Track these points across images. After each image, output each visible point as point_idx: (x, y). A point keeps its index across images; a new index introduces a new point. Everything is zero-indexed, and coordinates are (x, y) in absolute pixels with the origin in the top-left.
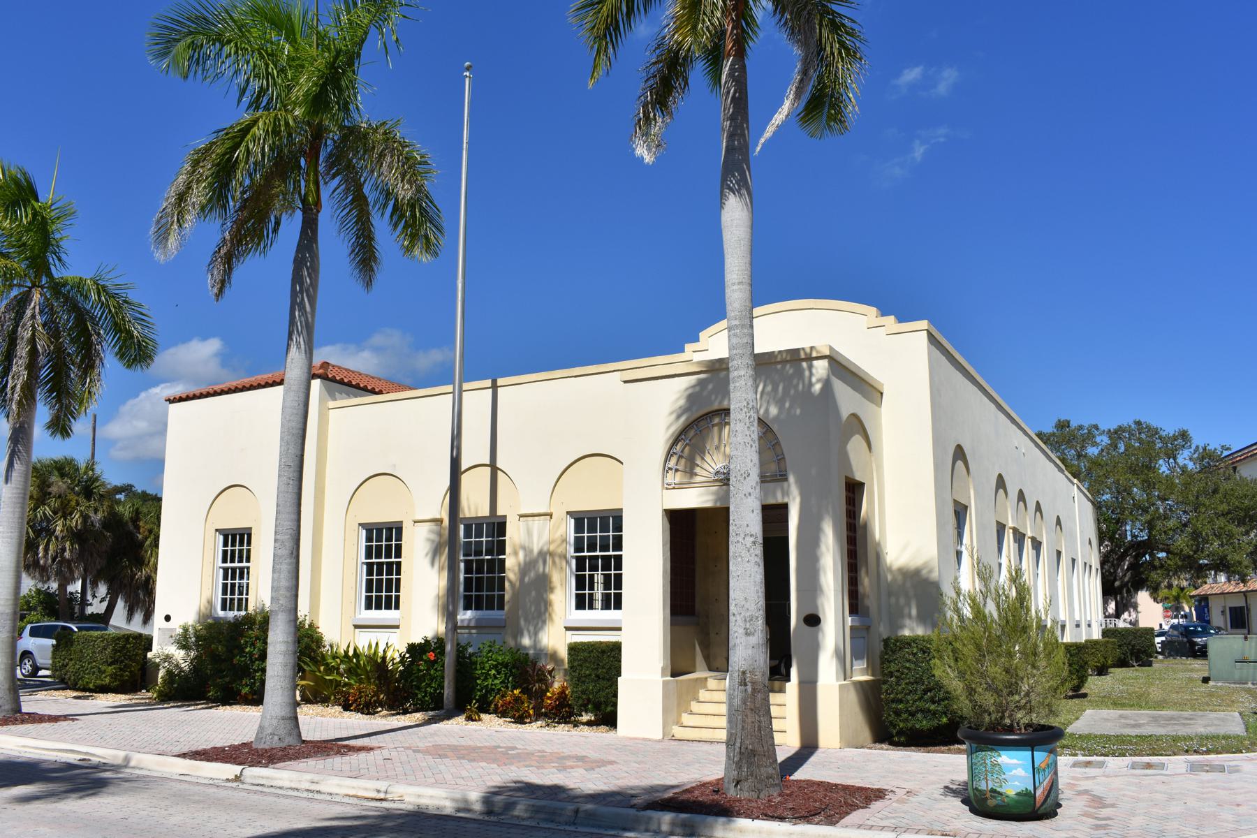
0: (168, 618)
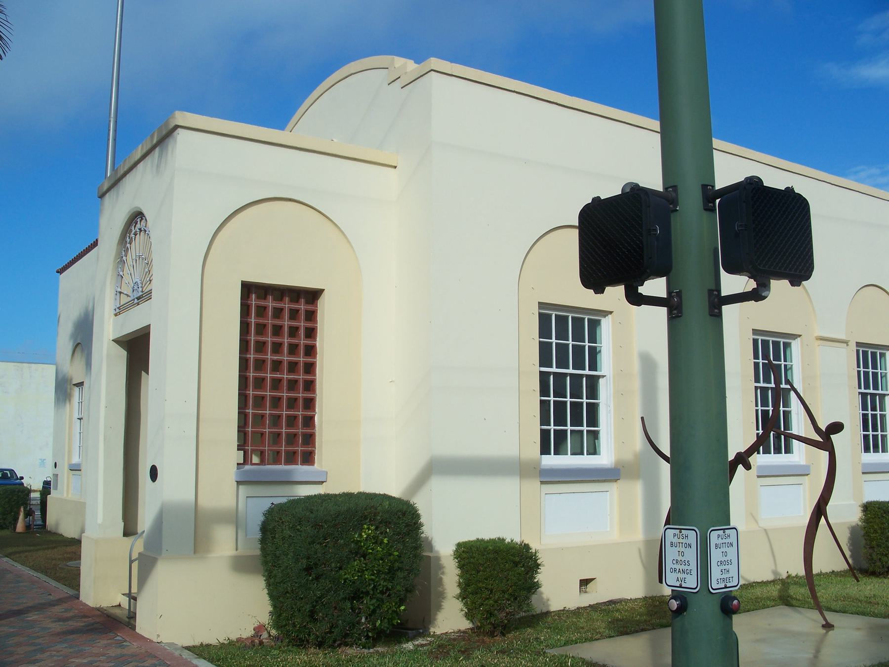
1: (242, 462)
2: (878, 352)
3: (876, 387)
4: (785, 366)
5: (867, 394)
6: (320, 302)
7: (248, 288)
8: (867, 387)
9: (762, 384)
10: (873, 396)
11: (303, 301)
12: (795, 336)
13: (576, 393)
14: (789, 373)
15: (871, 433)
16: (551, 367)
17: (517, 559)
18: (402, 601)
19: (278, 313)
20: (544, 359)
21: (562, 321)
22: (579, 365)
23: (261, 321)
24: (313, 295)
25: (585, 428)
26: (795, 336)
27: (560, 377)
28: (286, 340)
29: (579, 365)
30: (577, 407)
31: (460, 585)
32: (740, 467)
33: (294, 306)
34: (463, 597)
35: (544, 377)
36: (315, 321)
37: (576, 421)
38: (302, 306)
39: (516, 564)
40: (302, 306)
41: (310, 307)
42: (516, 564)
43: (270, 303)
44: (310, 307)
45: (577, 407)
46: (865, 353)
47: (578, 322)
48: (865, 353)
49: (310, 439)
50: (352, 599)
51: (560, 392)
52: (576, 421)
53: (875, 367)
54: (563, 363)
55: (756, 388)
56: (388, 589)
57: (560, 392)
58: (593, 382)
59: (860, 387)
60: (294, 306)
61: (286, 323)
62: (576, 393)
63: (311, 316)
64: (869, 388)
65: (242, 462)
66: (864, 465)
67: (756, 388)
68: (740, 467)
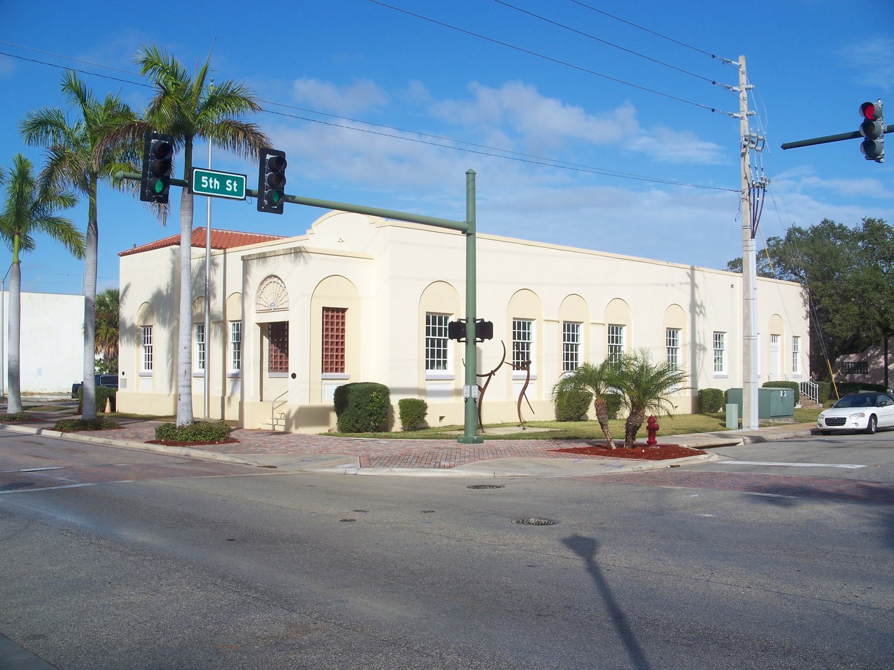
0: (123, 373)
1: (527, 371)
2: (517, 321)
3: (573, 341)
4: (577, 335)
5: (617, 346)
6: (346, 313)
7: (324, 309)
8: (670, 345)
9: (566, 342)
10: (672, 348)
11: (340, 313)
12: (533, 320)
13: (439, 346)
14: (621, 339)
15: (570, 361)
16: (436, 336)
17: (420, 405)
18: (384, 418)
19: (332, 316)
20: (428, 334)
21: (434, 318)
22: (524, 339)
23: (327, 320)
24: (344, 310)
25: (442, 359)
26: (533, 320)
27: (433, 340)
28: (335, 327)
29: (613, 342)
30: (439, 351)
31: (400, 414)
32: (493, 375)
33: (338, 314)
34: (402, 418)
35: (427, 339)
36: (345, 320)
37: (439, 356)
38: (340, 314)
39: (420, 406)
40: (340, 314)
41: (343, 314)
42: (420, 406)
43: (335, 314)
44: (343, 314)
45: (439, 351)
46: (716, 335)
47: (524, 323)
48: (716, 335)
49: (343, 363)
50: (369, 416)
51: (433, 345)
52: (439, 356)
53: (673, 337)
54: (434, 334)
55: (514, 342)
56: (380, 413)
57: (433, 345)
58: (528, 344)
59: (609, 343)
60: (338, 314)
61: (335, 321)
62: (439, 346)
63: (343, 317)
64: (614, 343)
65: (527, 371)
66: (514, 376)
67: (564, 344)
68: (493, 375)
